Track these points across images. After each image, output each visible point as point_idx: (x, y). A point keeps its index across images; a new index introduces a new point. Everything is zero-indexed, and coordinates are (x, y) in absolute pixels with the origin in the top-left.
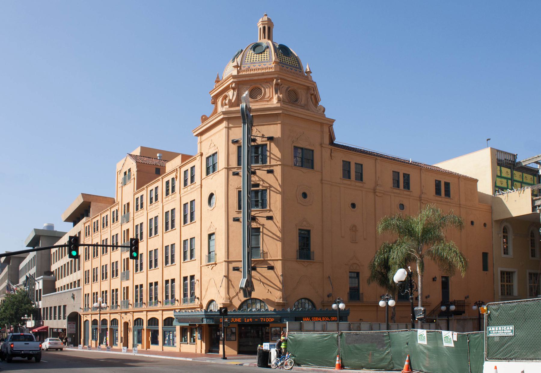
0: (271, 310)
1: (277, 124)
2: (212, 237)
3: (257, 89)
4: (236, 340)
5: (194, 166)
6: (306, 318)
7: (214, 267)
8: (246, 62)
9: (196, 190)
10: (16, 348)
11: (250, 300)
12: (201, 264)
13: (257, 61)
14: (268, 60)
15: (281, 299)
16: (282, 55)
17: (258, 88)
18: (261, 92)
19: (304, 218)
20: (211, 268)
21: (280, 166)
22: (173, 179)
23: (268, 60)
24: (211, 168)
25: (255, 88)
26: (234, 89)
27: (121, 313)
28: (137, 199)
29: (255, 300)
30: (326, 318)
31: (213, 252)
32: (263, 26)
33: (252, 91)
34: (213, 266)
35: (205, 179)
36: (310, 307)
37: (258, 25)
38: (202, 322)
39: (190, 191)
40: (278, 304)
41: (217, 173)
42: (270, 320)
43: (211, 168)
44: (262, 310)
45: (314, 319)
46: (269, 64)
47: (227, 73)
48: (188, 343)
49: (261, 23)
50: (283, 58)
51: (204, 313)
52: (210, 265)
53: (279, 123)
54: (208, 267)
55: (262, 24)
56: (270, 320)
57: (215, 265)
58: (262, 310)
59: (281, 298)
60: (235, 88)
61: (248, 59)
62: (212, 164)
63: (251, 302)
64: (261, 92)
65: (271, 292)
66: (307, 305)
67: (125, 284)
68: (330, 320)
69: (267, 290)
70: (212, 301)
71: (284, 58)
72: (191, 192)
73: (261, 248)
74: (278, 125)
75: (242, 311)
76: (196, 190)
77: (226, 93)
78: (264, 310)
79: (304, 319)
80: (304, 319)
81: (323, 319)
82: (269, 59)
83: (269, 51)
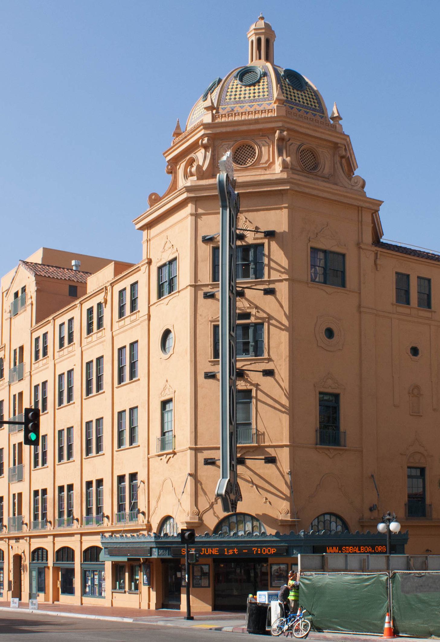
1: (281, 208)
2: (169, 407)
3: (247, 147)
4: (209, 586)
5: (137, 283)
7: (171, 458)
8: (228, 100)
9: (139, 324)
11: (235, 517)
13: (247, 98)
14: (266, 96)
15: (289, 515)
17: (249, 146)
20: (167, 459)
22: (99, 305)
23: (266, 96)
25: (244, 146)
26: (206, 147)
27: (9, 538)
28: (37, 339)
30: (366, 548)
31: (170, 433)
34: (170, 458)
35: (156, 304)
36: (340, 528)
38: (151, 556)
39: (129, 326)
40: (282, 524)
44: (254, 534)
45: (346, 549)
46: (268, 104)
48: (125, 592)
50: (292, 94)
52: (165, 456)
53: (285, 208)
54: (161, 459)
57: (173, 455)
58: (254, 534)
61: (231, 95)
62: (167, 279)
63: (237, 520)
64: (253, 153)
66: (333, 525)
67: (16, 488)
68: (373, 551)
73: (254, 426)
76: (139, 324)
77: (192, 155)
79: (329, 549)
80: (329, 549)
81: (362, 549)
82: (268, 95)
83: (267, 81)
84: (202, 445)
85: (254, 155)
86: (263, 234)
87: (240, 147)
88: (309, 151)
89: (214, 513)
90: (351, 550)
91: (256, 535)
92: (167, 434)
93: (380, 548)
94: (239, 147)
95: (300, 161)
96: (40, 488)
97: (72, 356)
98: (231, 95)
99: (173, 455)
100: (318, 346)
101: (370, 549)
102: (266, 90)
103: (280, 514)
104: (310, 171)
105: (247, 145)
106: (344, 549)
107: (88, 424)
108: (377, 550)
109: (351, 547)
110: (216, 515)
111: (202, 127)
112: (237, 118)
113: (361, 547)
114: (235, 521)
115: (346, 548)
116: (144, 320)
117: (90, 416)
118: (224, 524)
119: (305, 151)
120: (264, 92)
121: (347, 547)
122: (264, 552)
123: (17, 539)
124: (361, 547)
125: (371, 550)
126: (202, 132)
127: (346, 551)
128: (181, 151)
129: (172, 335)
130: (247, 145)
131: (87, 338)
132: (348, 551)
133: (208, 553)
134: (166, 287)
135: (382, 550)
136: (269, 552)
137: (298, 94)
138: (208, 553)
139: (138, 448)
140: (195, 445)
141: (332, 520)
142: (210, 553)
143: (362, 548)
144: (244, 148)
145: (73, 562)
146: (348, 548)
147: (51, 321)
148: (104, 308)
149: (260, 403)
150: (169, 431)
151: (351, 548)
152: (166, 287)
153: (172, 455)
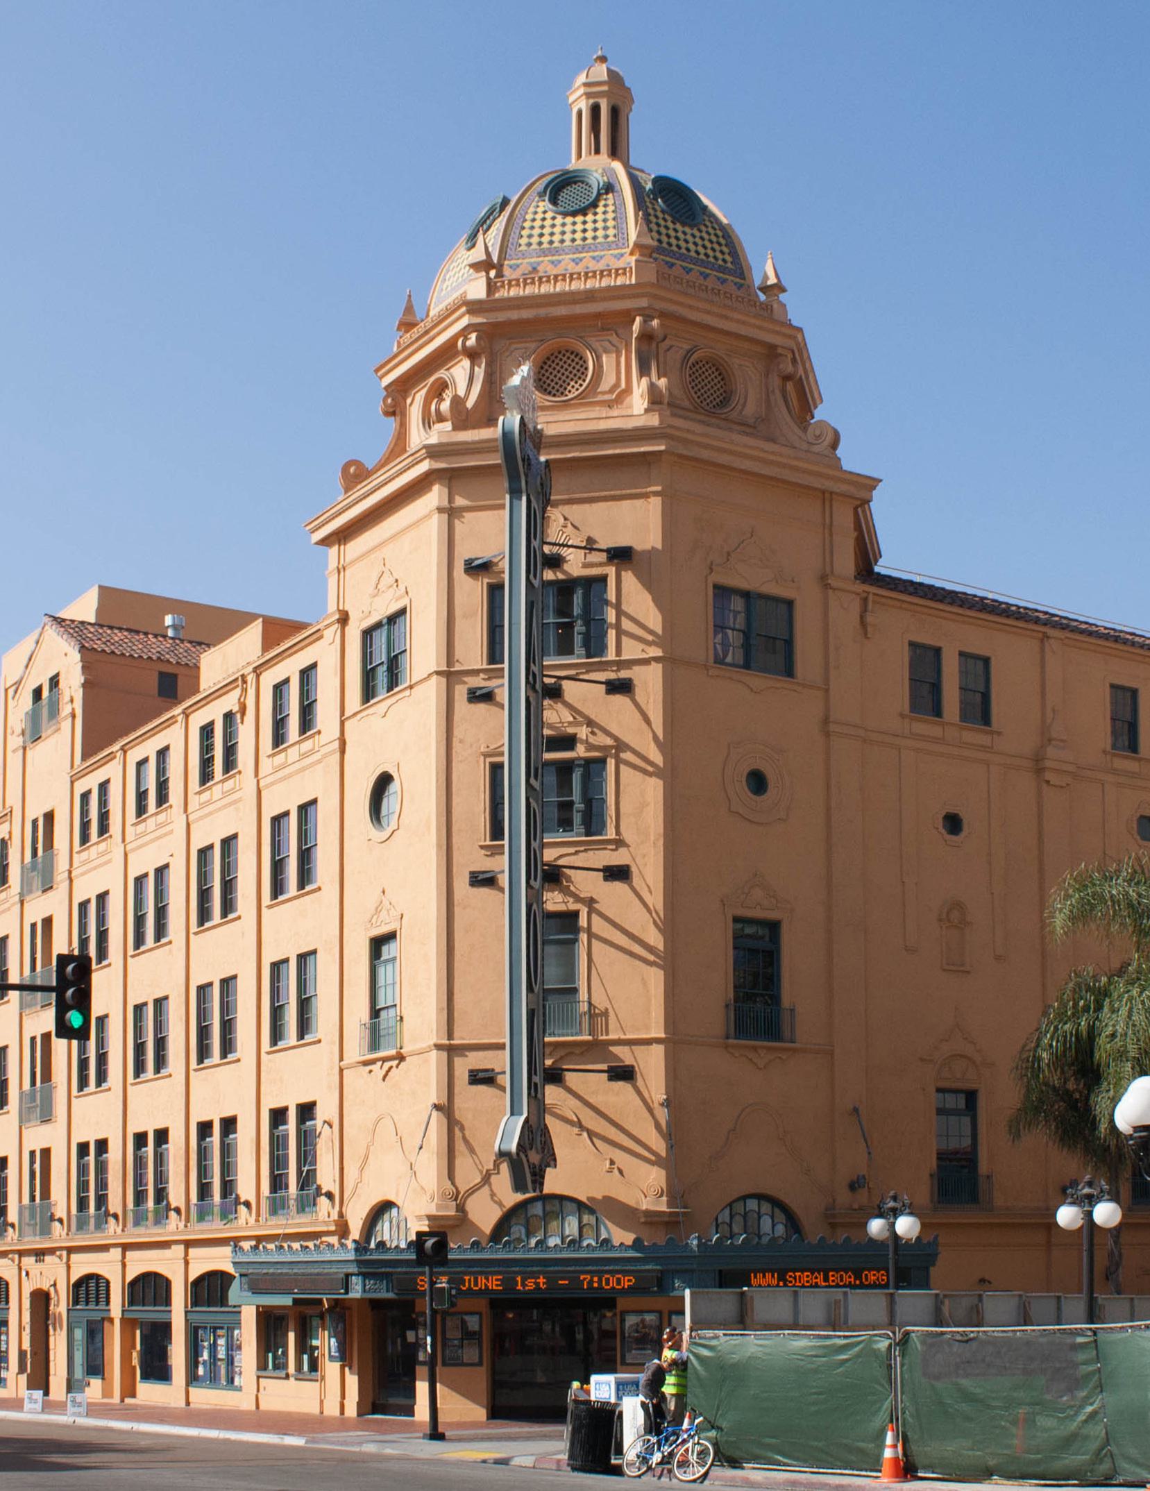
0: (622, 1244)
1: (645, 496)
2: (388, 951)
3: (568, 354)
4: (480, 1364)
5: (314, 666)
6: (764, 1276)
7: (394, 1068)
8: (523, 248)
11: (539, 1205)
12: (341, 1059)
13: (568, 243)
14: (611, 239)
15: (664, 1198)
16: (665, 220)
17: (572, 353)
20: (383, 1072)
21: (660, 665)
22: (229, 717)
23: (611, 239)
24: (382, 674)
25: (560, 353)
26: (473, 355)
27: (21, 1253)
28: (85, 796)
29: (556, 1202)
30: (841, 1276)
31: (392, 1011)
34: (391, 1067)
36: (780, 1230)
38: (347, 1293)
40: (649, 1219)
41: (407, 693)
42: (619, 1283)
43: (382, 674)
44: (585, 1244)
45: (795, 1278)
47: (444, 292)
48: (287, 1377)
51: (353, 1253)
52: (379, 1063)
53: (656, 494)
56: (619, 1283)
57: (397, 1062)
59: (661, 1196)
61: (530, 236)
62: (384, 658)
63: (544, 1210)
64: (582, 370)
65: (621, 1172)
66: (766, 1223)
67: (38, 1137)
68: (858, 1282)
69: (608, 1162)
70: (384, 1207)
71: (676, 230)
72: (303, 769)
73: (583, 995)
76: (319, 762)
77: (442, 374)
78: (594, 1244)
79: (755, 1277)
80: (755, 1277)
81: (831, 1279)
82: (615, 236)
83: (614, 204)
84: (463, 1039)
86: (604, 555)
88: (710, 364)
91: (588, 1245)
92: (383, 1014)
95: (688, 379)
96: (91, 1138)
97: (165, 835)
98: (530, 236)
99: (397, 1062)
101: (850, 1277)
102: (611, 223)
104: (713, 410)
105: (567, 351)
107: (203, 989)
108: (867, 1280)
109: (806, 1274)
111: (464, 309)
112: (545, 289)
113: (831, 1273)
114: (540, 1213)
116: (331, 753)
117: (208, 972)
118: (514, 1220)
119: (701, 364)
120: (606, 228)
121: (798, 1274)
123: (40, 1254)
124: (831, 1273)
126: (465, 321)
129: (394, 787)
130: (567, 351)
131: (200, 793)
134: (382, 676)
137: (685, 233)
139: (317, 1045)
140: (449, 1039)
141: (763, 1210)
143: (833, 1276)
144: (560, 356)
147: (118, 754)
150: (387, 1008)
151: (808, 1276)
152: (382, 676)
153: (395, 1063)
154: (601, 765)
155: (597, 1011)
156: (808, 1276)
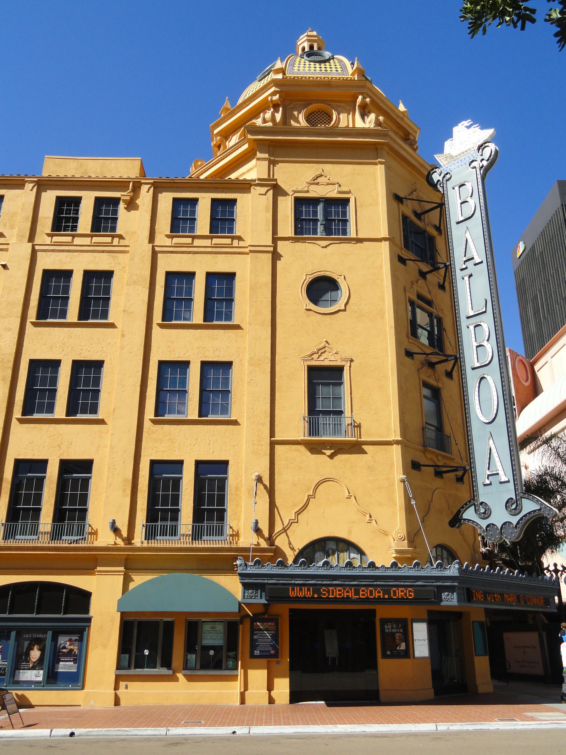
0: (383, 566)
1: (375, 164)
3: (323, 113)
10: (243, 629)
12: (271, 437)
15: (406, 541)
17: (325, 113)
18: (329, 121)
19: (252, 453)
21: (388, 242)
25: (319, 111)
26: (276, 106)
32: (310, 43)
33: (313, 113)
37: (299, 43)
42: (371, 594)
49: (306, 38)
53: (381, 163)
55: (308, 41)
56: (371, 594)
59: (404, 540)
60: (280, 103)
64: (329, 121)
69: (368, 516)
73: (347, 413)
74: (379, 166)
75: (301, 565)
81: (361, 593)
85: (329, 123)
87: (315, 111)
89: (289, 543)
90: (338, 593)
93: (402, 591)
94: (313, 111)
100: (410, 342)
101: (379, 592)
103: (392, 540)
105: (323, 112)
106: (324, 590)
109: (400, 589)
110: (291, 546)
111: (273, 84)
115: (329, 590)
122: (395, 595)
125: (381, 594)
126: (273, 89)
127: (329, 595)
128: (248, 110)
130: (323, 112)
132: (333, 595)
133: (396, 596)
135: (406, 594)
136: (370, 595)
138: (396, 596)
142: (400, 597)
143: (363, 591)
144: (319, 113)
145: (133, 666)
146: (333, 590)
148: (81, 708)
149: (425, 344)
151: (340, 591)
154: (179, 465)
155: (356, 424)
156: (340, 591)
